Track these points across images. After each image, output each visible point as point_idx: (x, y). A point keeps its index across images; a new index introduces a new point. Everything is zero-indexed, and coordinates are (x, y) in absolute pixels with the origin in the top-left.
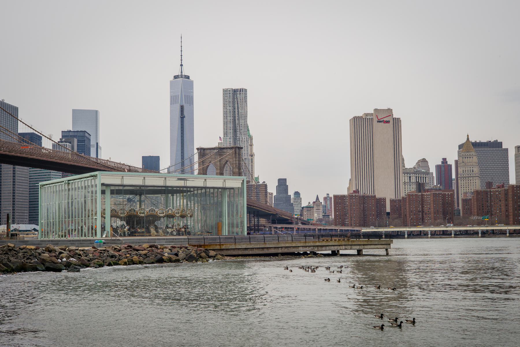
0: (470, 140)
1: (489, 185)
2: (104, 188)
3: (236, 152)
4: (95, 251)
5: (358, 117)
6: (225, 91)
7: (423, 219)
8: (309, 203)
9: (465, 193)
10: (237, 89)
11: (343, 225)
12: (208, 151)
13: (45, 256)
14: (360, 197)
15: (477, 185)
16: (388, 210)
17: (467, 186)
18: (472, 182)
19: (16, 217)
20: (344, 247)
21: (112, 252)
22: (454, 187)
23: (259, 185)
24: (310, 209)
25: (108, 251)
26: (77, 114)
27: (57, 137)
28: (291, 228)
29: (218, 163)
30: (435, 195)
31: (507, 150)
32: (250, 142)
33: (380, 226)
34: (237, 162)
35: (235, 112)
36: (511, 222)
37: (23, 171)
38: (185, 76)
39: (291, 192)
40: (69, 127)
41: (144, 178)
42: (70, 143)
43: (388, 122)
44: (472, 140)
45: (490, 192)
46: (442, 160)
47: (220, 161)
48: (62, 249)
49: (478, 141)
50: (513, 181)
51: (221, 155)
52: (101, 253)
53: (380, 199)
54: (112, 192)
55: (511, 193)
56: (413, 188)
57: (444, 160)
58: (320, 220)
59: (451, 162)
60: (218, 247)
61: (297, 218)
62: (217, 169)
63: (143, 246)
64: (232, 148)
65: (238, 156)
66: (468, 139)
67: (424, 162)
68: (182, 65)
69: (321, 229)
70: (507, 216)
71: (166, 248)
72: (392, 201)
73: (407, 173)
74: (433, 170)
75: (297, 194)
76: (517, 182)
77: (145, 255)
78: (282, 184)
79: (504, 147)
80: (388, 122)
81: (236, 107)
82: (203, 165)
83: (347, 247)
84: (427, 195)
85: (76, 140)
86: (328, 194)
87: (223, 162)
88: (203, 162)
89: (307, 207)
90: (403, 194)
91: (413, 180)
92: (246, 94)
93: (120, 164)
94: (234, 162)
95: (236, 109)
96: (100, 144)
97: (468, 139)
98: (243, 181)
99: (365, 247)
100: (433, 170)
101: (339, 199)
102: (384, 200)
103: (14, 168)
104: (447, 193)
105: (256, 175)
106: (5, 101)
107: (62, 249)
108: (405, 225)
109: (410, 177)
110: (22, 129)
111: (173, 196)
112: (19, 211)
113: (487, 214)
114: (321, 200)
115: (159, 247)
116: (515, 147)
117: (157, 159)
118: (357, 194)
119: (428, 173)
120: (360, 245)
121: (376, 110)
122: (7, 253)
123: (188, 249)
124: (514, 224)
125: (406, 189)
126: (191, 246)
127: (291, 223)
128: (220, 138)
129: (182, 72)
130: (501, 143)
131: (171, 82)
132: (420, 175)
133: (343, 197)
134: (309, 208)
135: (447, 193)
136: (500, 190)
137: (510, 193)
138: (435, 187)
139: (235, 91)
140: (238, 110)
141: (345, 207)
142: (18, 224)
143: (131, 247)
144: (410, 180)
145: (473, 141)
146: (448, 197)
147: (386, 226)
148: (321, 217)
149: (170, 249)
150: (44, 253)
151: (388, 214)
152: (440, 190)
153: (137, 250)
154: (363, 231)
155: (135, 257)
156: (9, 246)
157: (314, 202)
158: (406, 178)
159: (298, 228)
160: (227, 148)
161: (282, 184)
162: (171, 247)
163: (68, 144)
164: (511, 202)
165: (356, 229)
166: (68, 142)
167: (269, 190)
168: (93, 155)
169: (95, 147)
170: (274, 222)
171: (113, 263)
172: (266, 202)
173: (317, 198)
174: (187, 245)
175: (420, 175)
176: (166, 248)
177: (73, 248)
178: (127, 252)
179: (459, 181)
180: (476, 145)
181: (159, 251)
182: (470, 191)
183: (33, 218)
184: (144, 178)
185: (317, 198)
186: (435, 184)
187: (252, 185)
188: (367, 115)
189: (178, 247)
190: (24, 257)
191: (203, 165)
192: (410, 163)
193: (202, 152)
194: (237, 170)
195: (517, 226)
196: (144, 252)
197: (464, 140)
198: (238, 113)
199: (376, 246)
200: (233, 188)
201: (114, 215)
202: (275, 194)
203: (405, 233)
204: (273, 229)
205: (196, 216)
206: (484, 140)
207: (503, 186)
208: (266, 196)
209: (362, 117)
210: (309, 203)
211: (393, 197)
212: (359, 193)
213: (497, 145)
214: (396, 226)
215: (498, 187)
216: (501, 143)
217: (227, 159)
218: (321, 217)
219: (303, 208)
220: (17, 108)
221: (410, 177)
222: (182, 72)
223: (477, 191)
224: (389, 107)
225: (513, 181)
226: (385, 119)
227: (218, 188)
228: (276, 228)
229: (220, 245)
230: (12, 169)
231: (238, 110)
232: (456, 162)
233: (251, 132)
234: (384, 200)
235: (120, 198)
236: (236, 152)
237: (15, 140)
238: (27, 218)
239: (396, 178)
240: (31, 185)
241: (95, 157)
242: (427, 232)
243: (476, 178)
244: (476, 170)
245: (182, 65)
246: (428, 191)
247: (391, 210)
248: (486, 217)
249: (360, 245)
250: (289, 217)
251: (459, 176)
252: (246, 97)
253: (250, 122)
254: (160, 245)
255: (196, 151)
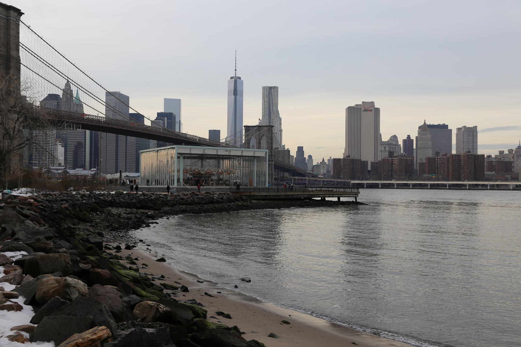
0: (426, 123)
1: (437, 154)
2: (179, 155)
3: (269, 129)
4: (171, 195)
5: (352, 107)
6: (264, 88)
7: (392, 175)
8: (318, 163)
9: (421, 159)
10: (272, 87)
11: (340, 178)
12: (251, 128)
13: (142, 198)
14: (351, 160)
15: (430, 154)
16: (369, 169)
17: (423, 154)
18: (426, 151)
19: (127, 168)
20: (328, 196)
21: (182, 196)
22: (415, 155)
23: (284, 150)
24: (318, 167)
25: (180, 196)
26: (167, 101)
27: (154, 117)
28: (305, 179)
29: (258, 136)
30: (400, 160)
31: (451, 130)
32: (279, 122)
33: (362, 180)
34: (270, 136)
35: (270, 102)
36: (451, 179)
37: (131, 139)
38: (238, 77)
39: (306, 156)
40: (162, 110)
41: (204, 150)
42: (162, 120)
43: (371, 110)
44: (428, 123)
45: (438, 158)
46: (407, 136)
47: (259, 134)
48: (151, 194)
49: (432, 124)
50: (454, 152)
51: (259, 131)
52: (175, 196)
53: (364, 162)
54: (184, 158)
55: (451, 160)
56: (386, 154)
57: (409, 137)
58: (324, 174)
59: (413, 137)
60: (248, 194)
61: (309, 173)
62: (257, 140)
63: (202, 192)
64: (267, 126)
65: (270, 132)
66: (425, 123)
67: (395, 137)
68: (236, 70)
69: (324, 180)
70: (448, 175)
71: (216, 194)
72: (372, 163)
73: (383, 145)
74: (401, 143)
75: (310, 157)
76: (457, 152)
77: (202, 198)
78: (300, 150)
79: (449, 128)
80: (371, 110)
81: (271, 99)
82: (248, 137)
83: (330, 196)
84: (395, 160)
85: (166, 118)
86: (331, 157)
87: (261, 135)
88: (248, 135)
89: (316, 165)
90: (380, 159)
91: (387, 149)
92: (278, 90)
93: (193, 136)
94: (268, 136)
95: (271, 100)
96: (182, 122)
97: (425, 123)
98: (266, 152)
99: (342, 196)
100: (401, 143)
101: (336, 161)
102: (367, 162)
103: (126, 138)
104: (408, 159)
105: (283, 144)
106: (121, 92)
107: (151, 194)
108: (380, 180)
109: (385, 147)
110: (131, 111)
111: (223, 160)
112: (130, 164)
113: (435, 173)
114: (326, 161)
115: (212, 193)
116: (457, 129)
117: (219, 132)
118: (349, 158)
119: (397, 145)
120: (339, 194)
121: (363, 102)
122: (119, 196)
123: (229, 195)
124: (452, 180)
125: (382, 155)
126: (231, 193)
127: (305, 176)
128: (259, 119)
129: (236, 75)
130: (448, 125)
131: (229, 81)
132: (393, 147)
133: (339, 160)
134: (318, 166)
135: (408, 159)
136: (444, 157)
137: (451, 160)
138: (401, 154)
139: (270, 88)
140: (272, 100)
141: (341, 166)
142: (129, 172)
143: (194, 193)
144: (385, 149)
145: (428, 124)
146: (409, 162)
147: (367, 180)
148: (325, 172)
149: (218, 195)
150: (141, 196)
151: (369, 171)
152: (404, 156)
153: (198, 195)
154: (351, 182)
155: (196, 199)
156: (120, 192)
157: (321, 163)
158: (382, 148)
159: (309, 180)
160: (263, 126)
161: (300, 150)
162: (219, 193)
163: (161, 121)
164: (451, 166)
165: (347, 181)
166: (161, 120)
167: (291, 154)
168: (177, 130)
169: (179, 123)
170: (293, 176)
171: (183, 203)
172: (289, 162)
173: (323, 160)
174: (229, 193)
175: (395, 147)
176: (216, 194)
177: (158, 193)
178: (192, 196)
179: (418, 151)
180: (430, 126)
181: (211, 196)
182: (425, 157)
183: (137, 170)
184: (204, 150)
185: (323, 160)
186: (402, 152)
187: (280, 150)
188: (357, 105)
189: (223, 194)
190: (129, 199)
191: (248, 137)
192: (385, 138)
193: (247, 128)
194: (270, 141)
195: (451, 182)
196: (202, 196)
197: (422, 124)
198: (272, 103)
199: (349, 196)
200: (259, 157)
201: (185, 171)
202: (295, 156)
203: (410, 184)
204: (293, 180)
205: (237, 173)
206: (436, 123)
207: (446, 155)
208: (289, 158)
209: (354, 107)
210: (318, 163)
211: (373, 161)
212: (350, 157)
213: (445, 127)
214: (373, 180)
215: (443, 156)
216: (448, 125)
217: (263, 133)
218: (325, 172)
219: (313, 166)
220: (129, 97)
221: (385, 147)
222: (236, 75)
223: (429, 158)
224: (372, 101)
225: (454, 152)
226: (370, 109)
227: (251, 157)
228: (295, 179)
229: (250, 193)
230: (125, 139)
231: (272, 100)
232: (417, 137)
233: (281, 116)
234: (367, 162)
235: (189, 161)
236: (269, 129)
237: (127, 119)
238: (134, 169)
239: (376, 148)
240: (138, 147)
241: (179, 131)
242: (394, 184)
243: (429, 149)
244: (430, 143)
245: (236, 70)
246: (396, 157)
247: (371, 169)
248: (434, 175)
249: (339, 194)
250: (303, 172)
251: (418, 147)
252: (277, 92)
253: (280, 108)
254: (212, 192)
255: (244, 128)
